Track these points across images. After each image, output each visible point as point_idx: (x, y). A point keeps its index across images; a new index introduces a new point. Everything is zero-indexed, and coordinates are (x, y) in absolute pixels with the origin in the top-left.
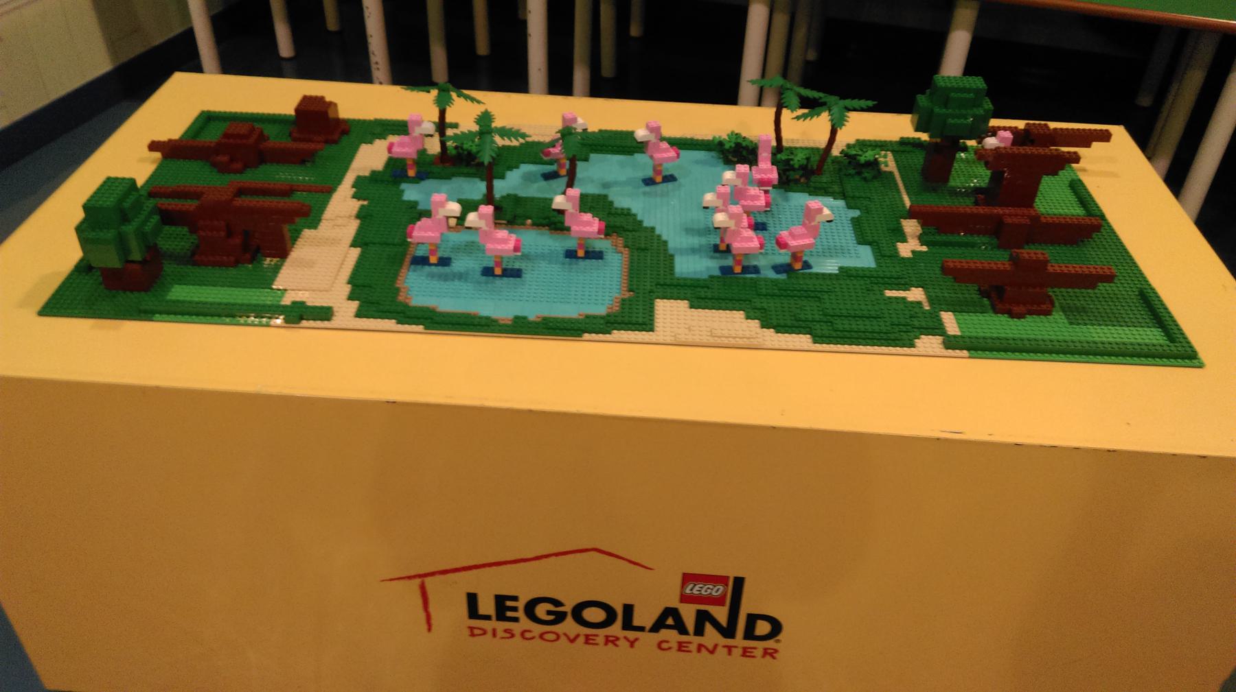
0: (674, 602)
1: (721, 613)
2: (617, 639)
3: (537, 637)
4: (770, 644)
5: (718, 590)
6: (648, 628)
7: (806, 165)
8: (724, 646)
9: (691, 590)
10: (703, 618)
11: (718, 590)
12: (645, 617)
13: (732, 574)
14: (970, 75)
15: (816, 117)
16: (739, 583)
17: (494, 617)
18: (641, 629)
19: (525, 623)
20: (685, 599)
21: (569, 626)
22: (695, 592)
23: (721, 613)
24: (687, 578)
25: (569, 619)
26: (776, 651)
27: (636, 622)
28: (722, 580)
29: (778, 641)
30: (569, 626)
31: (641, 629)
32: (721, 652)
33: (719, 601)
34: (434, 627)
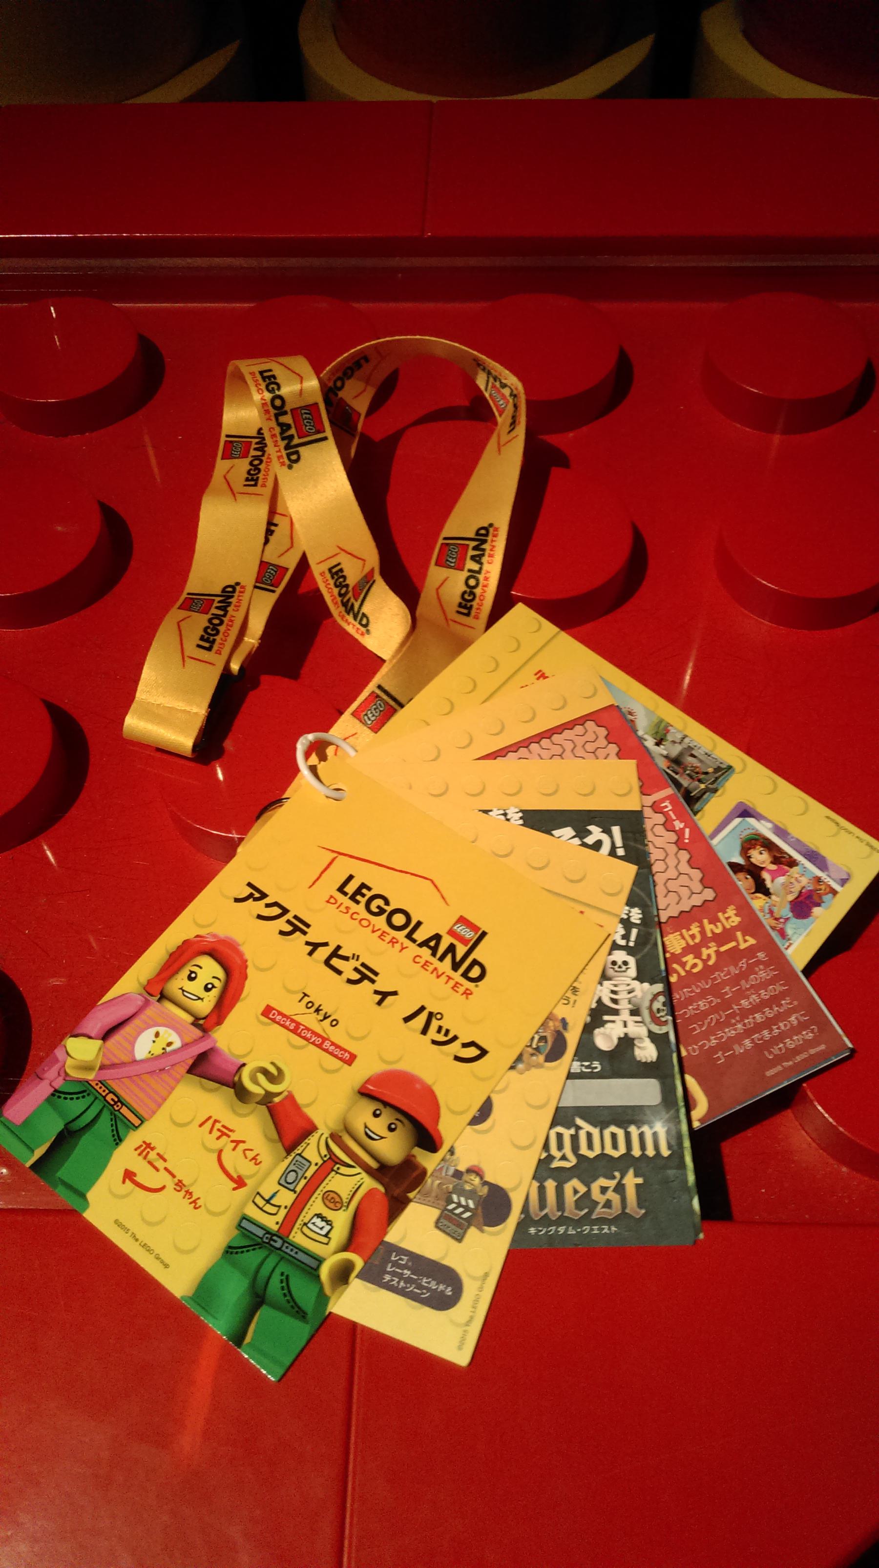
0: (443, 932)
1: (461, 950)
2: (397, 942)
3: (359, 920)
4: (471, 985)
5: (470, 934)
6: (418, 943)
7: (444, 1291)
8: (448, 976)
9: (461, 930)
10: (451, 949)
11: (470, 934)
12: (421, 935)
13: (484, 928)
14: (361, 1279)
15: (601, 830)
16: (484, 934)
17: (349, 896)
18: (414, 941)
19: (361, 908)
20: (451, 933)
21: (382, 920)
22: (458, 930)
23: (461, 950)
24: (462, 920)
25: (385, 916)
26: (326, 1013)
27: (415, 936)
28: (474, 927)
29: (477, 986)
30: (382, 920)
31: (414, 941)
32: (444, 978)
33: (464, 941)
34: (311, 888)
